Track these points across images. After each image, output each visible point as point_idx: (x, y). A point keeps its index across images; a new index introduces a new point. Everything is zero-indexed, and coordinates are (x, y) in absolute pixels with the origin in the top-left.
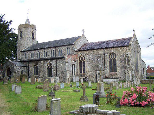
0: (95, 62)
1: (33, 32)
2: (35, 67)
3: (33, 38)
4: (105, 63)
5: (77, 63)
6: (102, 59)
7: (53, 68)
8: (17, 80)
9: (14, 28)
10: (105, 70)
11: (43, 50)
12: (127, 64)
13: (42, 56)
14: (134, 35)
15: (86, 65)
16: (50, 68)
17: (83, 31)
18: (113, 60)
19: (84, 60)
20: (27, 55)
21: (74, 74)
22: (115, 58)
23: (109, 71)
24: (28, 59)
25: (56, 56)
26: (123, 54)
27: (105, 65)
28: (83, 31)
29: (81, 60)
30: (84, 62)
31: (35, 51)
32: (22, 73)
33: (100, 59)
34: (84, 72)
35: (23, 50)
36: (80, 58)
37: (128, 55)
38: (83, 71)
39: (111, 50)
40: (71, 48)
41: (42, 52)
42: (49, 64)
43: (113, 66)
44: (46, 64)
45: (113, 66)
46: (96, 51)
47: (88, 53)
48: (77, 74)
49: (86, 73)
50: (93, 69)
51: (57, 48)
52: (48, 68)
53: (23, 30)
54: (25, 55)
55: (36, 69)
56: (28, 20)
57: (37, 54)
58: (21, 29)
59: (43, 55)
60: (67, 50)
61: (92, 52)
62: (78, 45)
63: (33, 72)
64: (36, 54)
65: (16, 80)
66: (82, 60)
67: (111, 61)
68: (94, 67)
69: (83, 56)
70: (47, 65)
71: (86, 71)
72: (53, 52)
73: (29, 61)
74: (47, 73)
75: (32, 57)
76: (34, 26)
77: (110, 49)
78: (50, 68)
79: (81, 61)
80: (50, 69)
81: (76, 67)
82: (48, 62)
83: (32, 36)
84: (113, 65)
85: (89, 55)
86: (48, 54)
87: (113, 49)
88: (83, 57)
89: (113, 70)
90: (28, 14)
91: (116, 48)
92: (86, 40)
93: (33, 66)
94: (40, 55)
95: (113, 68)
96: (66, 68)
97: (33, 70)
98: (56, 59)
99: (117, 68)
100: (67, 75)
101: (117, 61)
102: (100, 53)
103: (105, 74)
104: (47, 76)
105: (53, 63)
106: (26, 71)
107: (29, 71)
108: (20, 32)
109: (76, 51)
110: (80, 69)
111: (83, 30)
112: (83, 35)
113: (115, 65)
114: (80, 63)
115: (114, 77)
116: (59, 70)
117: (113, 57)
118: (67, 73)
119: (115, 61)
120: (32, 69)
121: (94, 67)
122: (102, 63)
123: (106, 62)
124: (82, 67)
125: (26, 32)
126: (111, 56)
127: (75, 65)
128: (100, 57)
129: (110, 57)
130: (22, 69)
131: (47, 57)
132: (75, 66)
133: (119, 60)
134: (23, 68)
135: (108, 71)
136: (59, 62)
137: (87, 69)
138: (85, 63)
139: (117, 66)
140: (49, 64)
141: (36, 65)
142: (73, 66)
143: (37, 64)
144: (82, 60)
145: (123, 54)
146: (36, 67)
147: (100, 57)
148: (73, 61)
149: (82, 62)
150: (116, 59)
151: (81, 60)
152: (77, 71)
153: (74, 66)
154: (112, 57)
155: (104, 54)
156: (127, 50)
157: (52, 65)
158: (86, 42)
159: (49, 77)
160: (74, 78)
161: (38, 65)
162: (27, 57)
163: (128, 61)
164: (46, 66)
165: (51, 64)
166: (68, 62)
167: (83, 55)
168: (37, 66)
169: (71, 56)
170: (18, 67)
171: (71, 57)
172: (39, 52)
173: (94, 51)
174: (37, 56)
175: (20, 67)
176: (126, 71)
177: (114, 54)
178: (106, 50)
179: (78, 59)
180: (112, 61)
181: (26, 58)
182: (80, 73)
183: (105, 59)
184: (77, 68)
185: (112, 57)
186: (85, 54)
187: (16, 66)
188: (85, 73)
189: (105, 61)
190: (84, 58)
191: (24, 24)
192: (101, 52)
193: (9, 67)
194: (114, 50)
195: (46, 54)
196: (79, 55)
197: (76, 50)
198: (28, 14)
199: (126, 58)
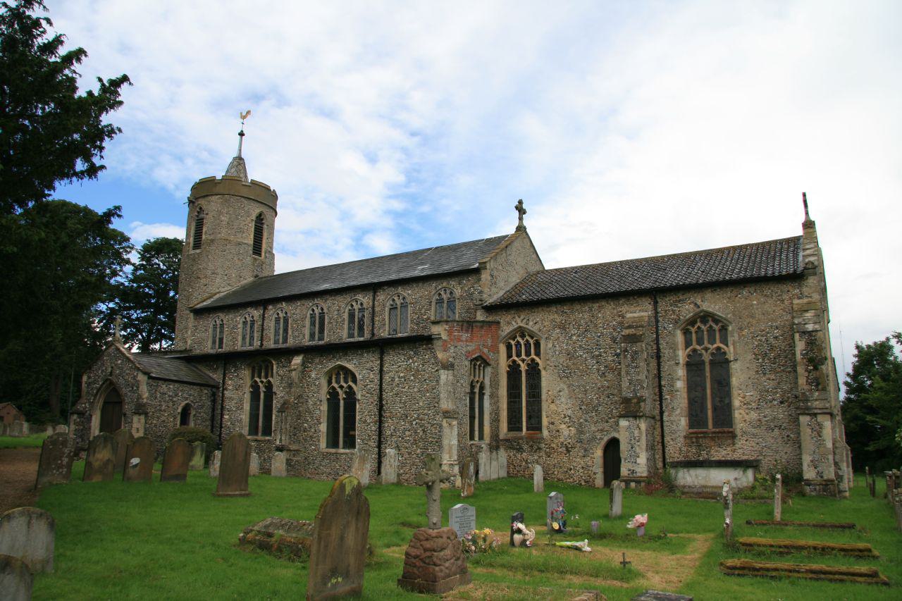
0: (598, 370)
1: (260, 219)
2: (255, 387)
3: (257, 249)
4: (659, 377)
5: (495, 375)
6: (644, 348)
7: (359, 396)
8: (135, 461)
9: (87, 82)
10: (662, 413)
11: (309, 303)
12: (802, 381)
13: (302, 335)
14: (809, 225)
15: (544, 383)
16: (342, 395)
17: (521, 210)
18: (707, 357)
19: (533, 360)
20: (222, 332)
21: (481, 438)
22: (534, 357)
23: (684, 422)
24: (226, 348)
25: (373, 334)
26: (772, 320)
27: (660, 386)
28: (521, 210)
29: (533, 356)
30: (534, 371)
31: (265, 309)
32: (184, 421)
33: (636, 352)
34: (535, 425)
35: (205, 303)
36: (509, 347)
37: (810, 327)
38: (529, 418)
39: (699, 302)
40: (458, 292)
41: (300, 313)
42: (338, 375)
43: (709, 391)
44: (318, 373)
45: (709, 391)
46: (607, 313)
47: (558, 318)
48: (495, 436)
49: (545, 433)
50: (588, 408)
51: (381, 296)
52: (333, 395)
53: (212, 206)
54: (211, 330)
55: (262, 401)
56: (239, 161)
57: (272, 324)
58: (202, 202)
59: (307, 332)
60: (440, 301)
61: (581, 315)
62: (495, 288)
63: (245, 417)
64: (270, 324)
65: (127, 462)
66: (523, 356)
67: (694, 365)
68: (592, 396)
69: (527, 337)
70: (324, 382)
71: (545, 421)
72: (361, 320)
73: (228, 360)
74: (323, 427)
75: (244, 338)
76: (267, 188)
77: (687, 295)
78: (342, 395)
79: (514, 361)
80: (342, 403)
81: (492, 396)
82: (331, 365)
83: (252, 236)
84: (712, 389)
85: (563, 327)
86: (330, 323)
87: (709, 295)
88: (531, 341)
89: (710, 413)
90: (242, 134)
91: (728, 293)
92: (534, 256)
93: (249, 382)
94: (290, 332)
95: (709, 405)
96: (437, 399)
97: (247, 407)
98: (381, 346)
99: (736, 403)
100: (445, 442)
101: (735, 367)
102: (629, 315)
103: (663, 436)
104: (323, 444)
105: (363, 368)
106: (205, 413)
107: (222, 408)
108: (197, 223)
109: (490, 309)
110: (509, 409)
111: (520, 202)
112: (521, 229)
113: (723, 385)
114: (514, 372)
115: (720, 454)
116: (394, 407)
117: (706, 337)
118: (446, 430)
119: (721, 363)
120: (241, 400)
121: (592, 396)
122: (643, 373)
123: (665, 367)
124: (528, 396)
125: (224, 218)
126: (514, 347)
127: (487, 382)
128: (633, 339)
129: (688, 343)
130: (185, 396)
131: (326, 339)
132: (487, 392)
133: (750, 357)
134: (194, 391)
135: (678, 422)
136: (397, 363)
137: (553, 407)
138: (543, 373)
139: (735, 392)
140: (338, 375)
141: (266, 377)
142: (477, 390)
143: (268, 370)
144: (523, 356)
145: (772, 320)
146: (262, 389)
147: (633, 339)
148: (476, 359)
149: (523, 367)
150: (730, 352)
151: (519, 355)
152: (495, 421)
153: (482, 388)
154: (519, 355)
155: (657, 321)
156: (796, 301)
157: (355, 381)
158: (534, 269)
159: (333, 451)
160: (483, 457)
161: (275, 381)
162: (221, 340)
163: (811, 361)
164: (319, 386)
165: (350, 375)
166: (449, 366)
167: (530, 326)
168: (269, 387)
169: (467, 331)
170: (164, 387)
171: (465, 336)
172: (281, 315)
173: (596, 306)
174: (270, 333)
175: (177, 385)
176: (804, 419)
177: (716, 321)
178: (664, 304)
179: (498, 352)
180: (703, 363)
181: (214, 342)
182: (510, 429)
183: (658, 349)
184: (496, 403)
185: (700, 342)
186: (536, 322)
187: (150, 377)
188: (539, 428)
189: (659, 365)
190: (537, 344)
191: (219, 177)
192: (639, 312)
193: (111, 383)
194: (713, 303)
195: (320, 323)
196: (506, 330)
197: (490, 301)
198: (242, 134)
199: (800, 346)
